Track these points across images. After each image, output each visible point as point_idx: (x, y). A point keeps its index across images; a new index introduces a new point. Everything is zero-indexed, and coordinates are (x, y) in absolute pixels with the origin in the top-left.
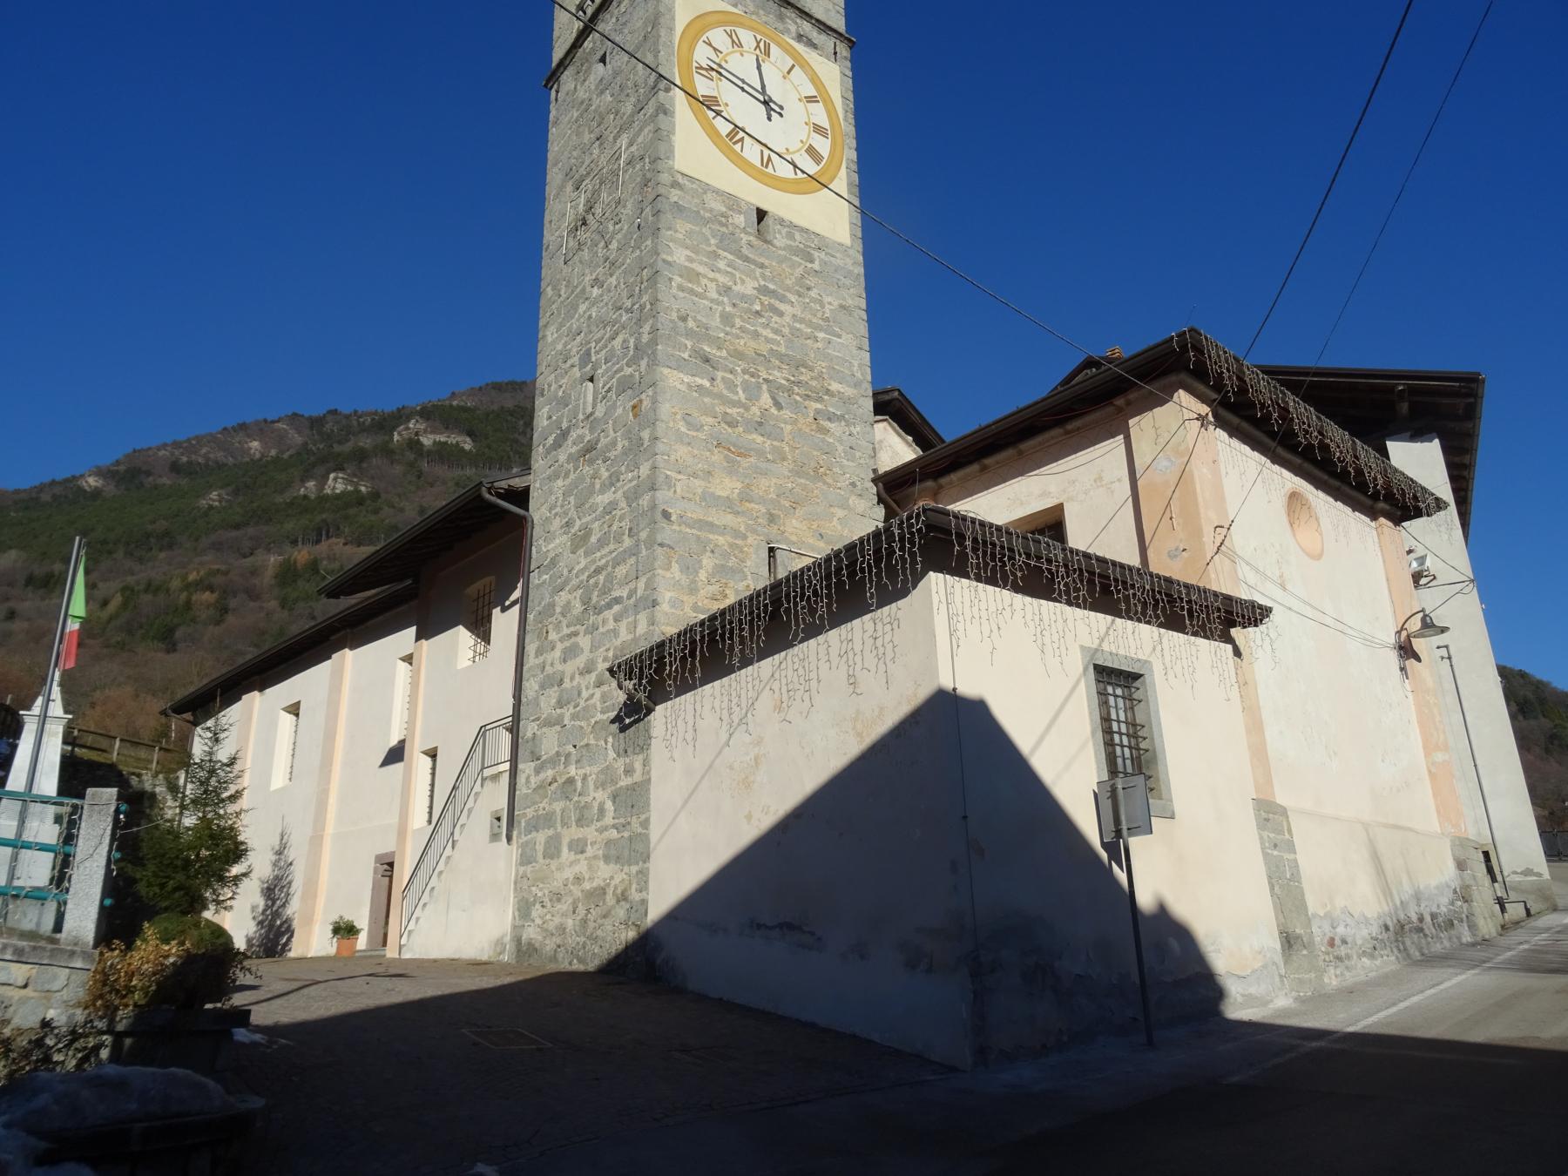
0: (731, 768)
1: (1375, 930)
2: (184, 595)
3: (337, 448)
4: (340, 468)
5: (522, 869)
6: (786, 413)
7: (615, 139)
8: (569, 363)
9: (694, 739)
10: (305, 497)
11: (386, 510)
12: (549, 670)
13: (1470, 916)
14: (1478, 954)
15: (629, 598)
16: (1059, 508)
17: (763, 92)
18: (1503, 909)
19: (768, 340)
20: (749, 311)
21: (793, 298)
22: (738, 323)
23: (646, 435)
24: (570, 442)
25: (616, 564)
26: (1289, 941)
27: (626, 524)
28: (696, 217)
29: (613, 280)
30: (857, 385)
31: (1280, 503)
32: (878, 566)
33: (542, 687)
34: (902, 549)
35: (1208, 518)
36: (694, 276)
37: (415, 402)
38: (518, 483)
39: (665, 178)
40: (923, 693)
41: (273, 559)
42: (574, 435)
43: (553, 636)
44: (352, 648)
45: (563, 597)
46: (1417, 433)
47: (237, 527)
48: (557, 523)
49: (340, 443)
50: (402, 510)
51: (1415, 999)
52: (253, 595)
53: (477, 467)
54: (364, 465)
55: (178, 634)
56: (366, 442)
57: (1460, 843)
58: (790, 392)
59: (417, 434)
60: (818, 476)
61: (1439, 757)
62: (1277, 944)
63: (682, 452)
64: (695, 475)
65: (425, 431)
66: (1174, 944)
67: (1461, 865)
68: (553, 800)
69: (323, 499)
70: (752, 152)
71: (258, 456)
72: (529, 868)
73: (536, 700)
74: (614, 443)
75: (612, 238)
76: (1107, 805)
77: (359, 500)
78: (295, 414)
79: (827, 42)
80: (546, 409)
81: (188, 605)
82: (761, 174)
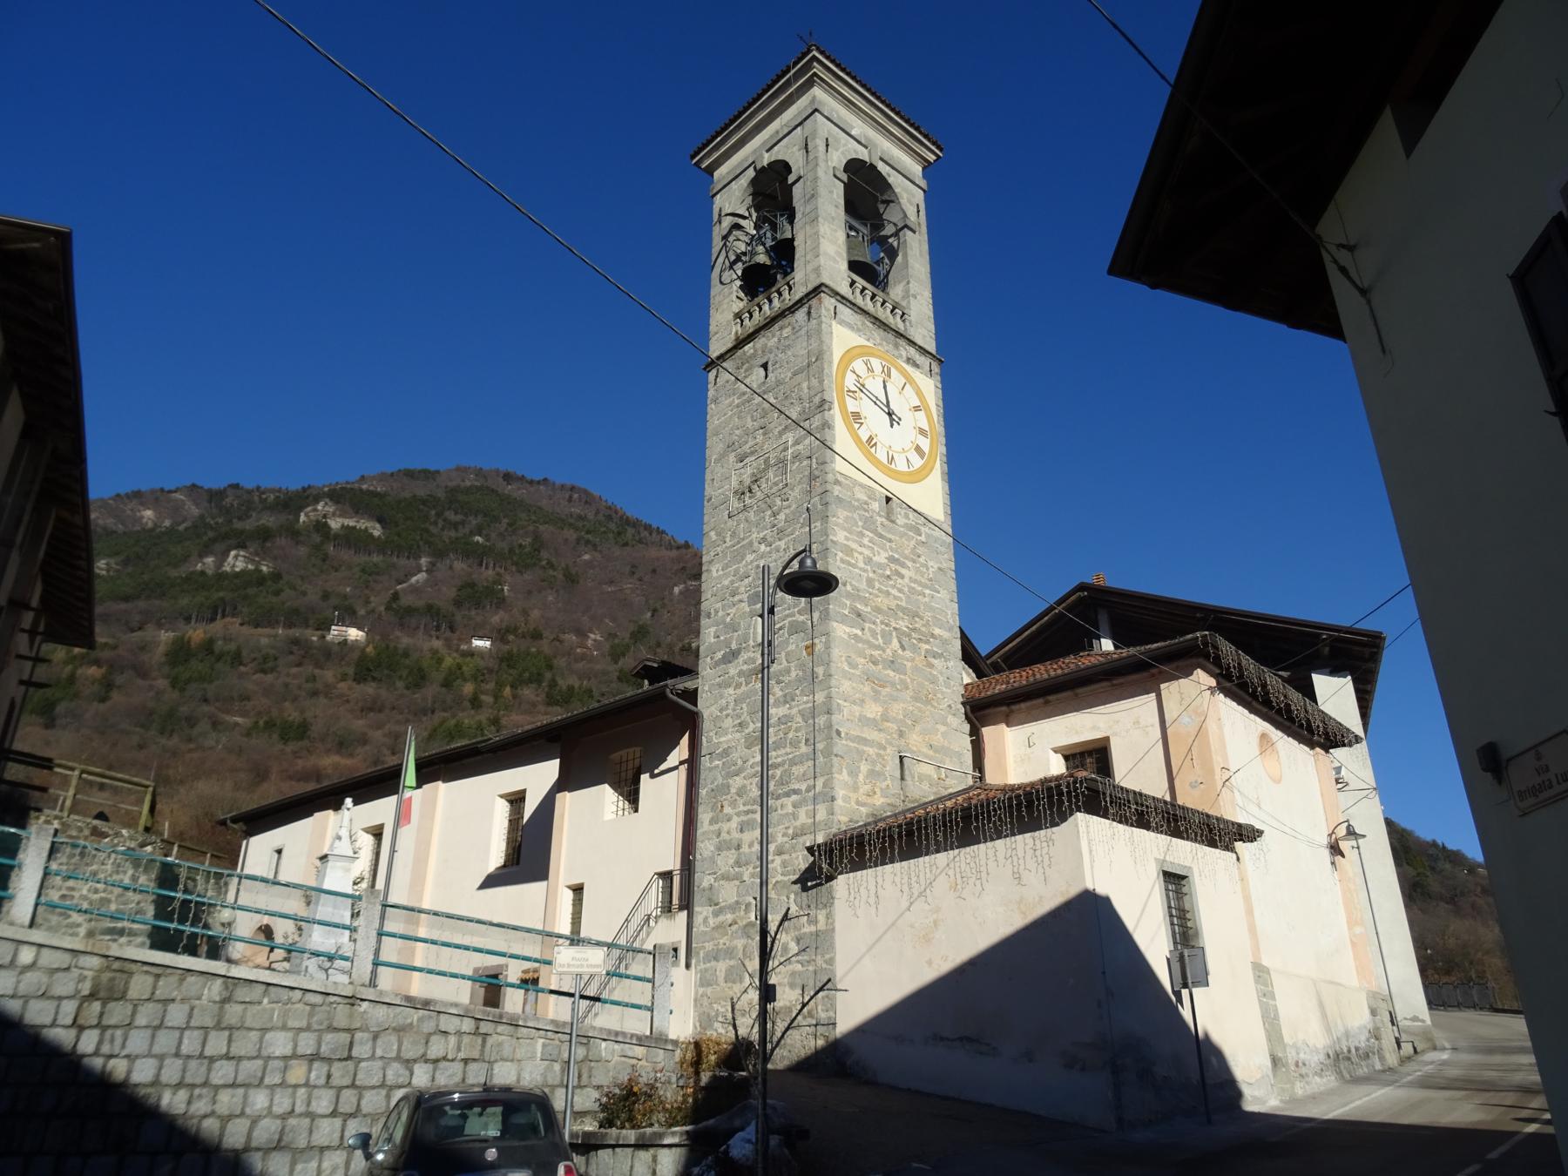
0: (912, 926)
1: (1322, 1057)
2: (69, 668)
3: (238, 525)
4: (241, 546)
5: (701, 990)
6: (908, 654)
7: (781, 434)
8: (737, 598)
9: (877, 903)
10: (203, 573)
11: (288, 593)
12: (724, 836)
13: (1380, 1049)
14: (1388, 1076)
15: (808, 790)
16: (1107, 739)
17: (888, 405)
18: (1399, 1047)
19: (896, 598)
20: (882, 576)
21: (909, 564)
22: (877, 585)
23: (820, 671)
24: (741, 660)
25: (793, 763)
26: (1276, 1061)
27: (802, 735)
28: (851, 507)
29: (782, 544)
30: (950, 629)
31: (1255, 741)
32: (1051, 809)
33: (719, 849)
34: (1069, 801)
35: (1218, 761)
36: (849, 551)
37: (322, 481)
38: (690, 685)
39: (830, 477)
40: (1073, 891)
41: (165, 636)
42: (744, 656)
43: (727, 810)
44: (445, 781)
45: (737, 782)
46: (1335, 671)
47: (126, 599)
48: (728, 723)
49: (240, 519)
50: (304, 594)
51: (1358, 1103)
52: (142, 672)
53: (384, 554)
54: (268, 544)
55: (60, 708)
56: (270, 520)
57: (1373, 996)
58: (909, 636)
59: (325, 516)
60: (928, 702)
61: (1358, 930)
62: (1269, 1063)
63: (846, 686)
64: (854, 703)
65: (334, 514)
66: (1214, 1060)
67: (1374, 1012)
68: (733, 938)
69: (221, 576)
70: (882, 456)
71: (150, 525)
72: (709, 990)
73: (713, 860)
74: (788, 671)
75: (780, 510)
76: (1176, 967)
77: (258, 579)
78: (194, 485)
79: (924, 361)
80: (713, 629)
81: (72, 679)
82: (888, 468)
